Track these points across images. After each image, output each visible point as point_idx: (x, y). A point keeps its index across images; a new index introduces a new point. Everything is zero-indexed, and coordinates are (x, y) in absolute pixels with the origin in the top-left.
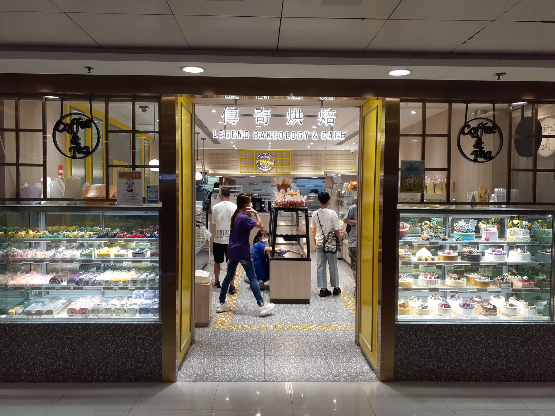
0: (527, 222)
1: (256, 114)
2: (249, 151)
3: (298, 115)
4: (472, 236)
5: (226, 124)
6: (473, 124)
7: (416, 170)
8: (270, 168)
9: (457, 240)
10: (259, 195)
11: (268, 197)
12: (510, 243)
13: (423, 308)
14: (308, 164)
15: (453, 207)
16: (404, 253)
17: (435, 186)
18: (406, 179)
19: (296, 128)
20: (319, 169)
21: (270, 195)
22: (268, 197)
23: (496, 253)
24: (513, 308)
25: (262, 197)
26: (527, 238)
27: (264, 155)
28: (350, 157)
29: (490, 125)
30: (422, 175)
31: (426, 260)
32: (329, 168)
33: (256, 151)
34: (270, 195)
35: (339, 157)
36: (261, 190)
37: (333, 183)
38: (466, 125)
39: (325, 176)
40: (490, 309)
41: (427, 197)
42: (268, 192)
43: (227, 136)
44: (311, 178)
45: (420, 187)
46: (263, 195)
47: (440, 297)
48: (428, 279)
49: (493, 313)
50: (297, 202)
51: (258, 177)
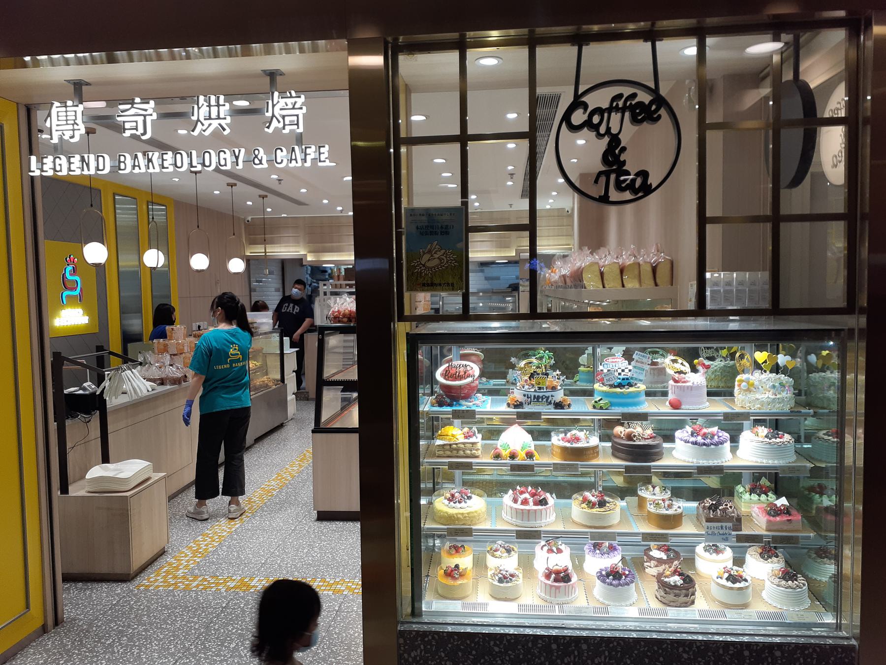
0: (788, 358)
3: (214, 110)
4: (637, 394)
6: (599, 99)
7: (449, 229)
9: (594, 407)
12: (738, 413)
13: (500, 581)
15: (548, 326)
16: (461, 439)
17: (622, 271)
18: (420, 257)
19: (218, 140)
20: (507, 246)
23: (699, 439)
24: (738, 585)
26: (781, 401)
29: (644, 97)
30: (461, 245)
31: (513, 456)
38: (577, 103)
39: (517, 259)
40: (675, 587)
41: (477, 304)
44: (493, 263)
45: (455, 274)
47: (563, 547)
48: (518, 506)
49: (682, 599)
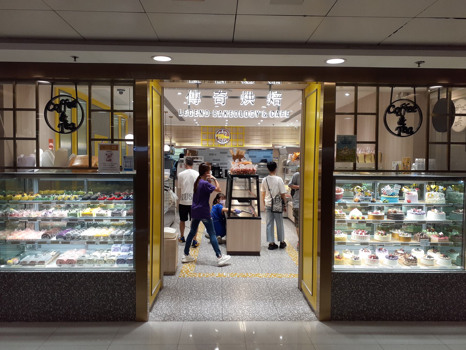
0: (443, 187)
1: (215, 96)
2: (209, 127)
3: (250, 97)
4: (396, 198)
5: (189, 104)
6: (398, 105)
7: (350, 143)
8: (227, 142)
9: (383, 202)
10: (218, 164)
11: (225, 165)
12: (428, 204)
13: (355, 259)
14: (259, 138)
15: (381, 174)
16: (339, 213)
17: (365, 156)
18: (341, 151)
19: (249, 108)
20: (268, 143)
21: (226, 164)
22: (225, 165)
23: (417, 212)
24: (431, 259)
25: (220, 166)
26: (442, 200)
27: (221, 130)
28: (294, 132)
29: (412, 105)
30: (354, 148)
31: (358, 218)
32: (276, 141)
33: (215, 127)
34: (226, 164)
35: (285, 132)
36: (219, 160)
37: (280, 154)
38: (391, 105)
39: (273, 148)
40: (411, 260)
41: (358, 166)
42: (225, 162)
43: (191, 114)
44: (261, 150)
45: (353, 157)
46: (221, 164)
47: (369, 250)
48: (359, 235)
49: (414, 264)
50: (250, 170)
51: (217, 149)
